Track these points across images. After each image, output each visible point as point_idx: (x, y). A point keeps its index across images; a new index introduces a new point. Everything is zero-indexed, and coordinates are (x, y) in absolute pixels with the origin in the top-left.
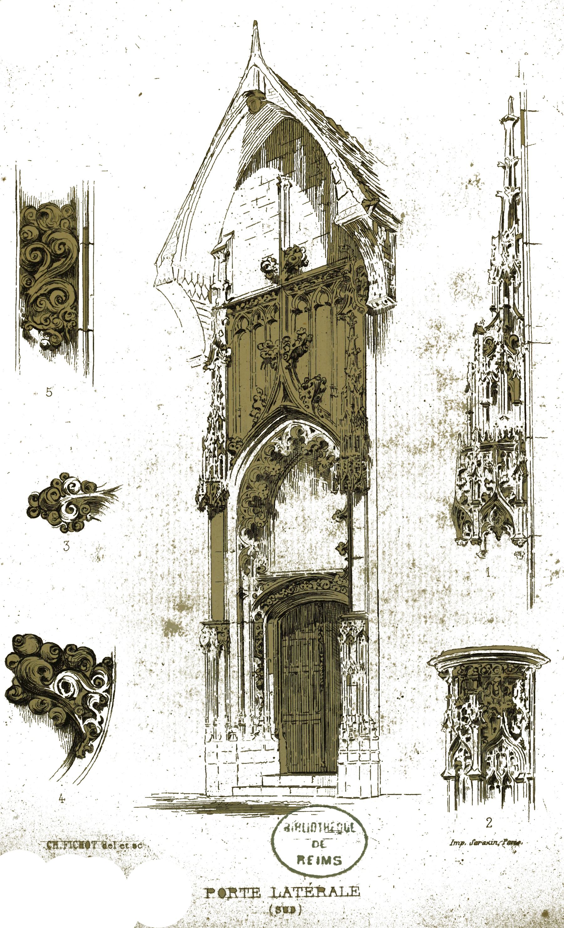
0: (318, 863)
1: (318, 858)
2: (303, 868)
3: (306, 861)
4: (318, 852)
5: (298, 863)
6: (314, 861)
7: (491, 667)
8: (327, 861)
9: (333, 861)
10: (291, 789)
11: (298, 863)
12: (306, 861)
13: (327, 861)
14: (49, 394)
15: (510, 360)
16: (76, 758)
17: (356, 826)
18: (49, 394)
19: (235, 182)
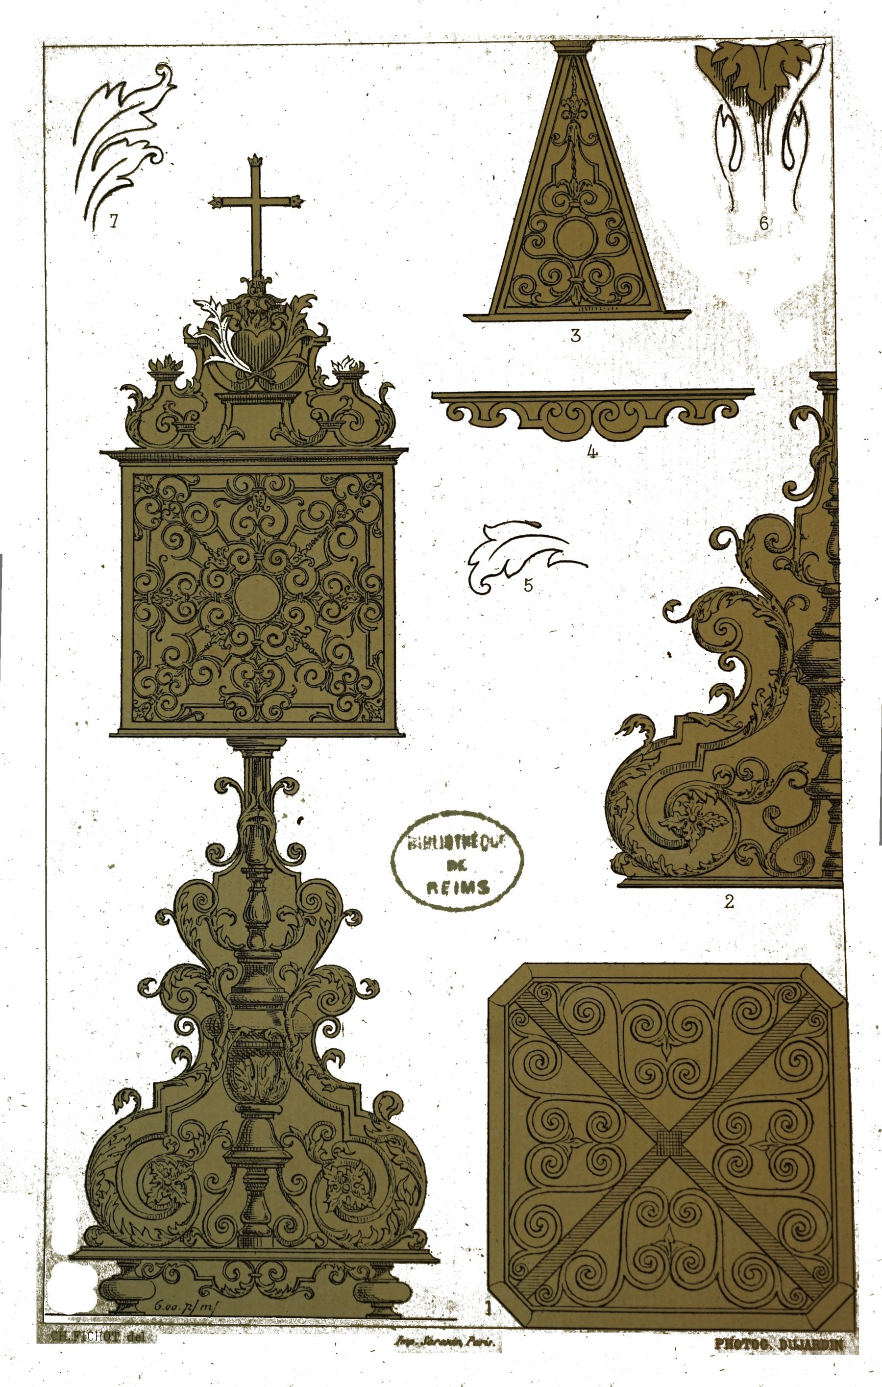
0: (456, 892)
1: (457, 884)
2: (436, 898)
3: (439, 888)
4: (457, 876)
5: (429, 893)
6: (451, 888)
7: (691, 821)
8: (467, 888)
9: (477, 888)
10: (738, 649)
11: (429, 893)
12: (439, 888)
13: (467, 888)
14: (528, 588)
15: (734, 722)
16: (717, 656)
17: (508, 840)
18: (528, 588)
19: (468, 313)
